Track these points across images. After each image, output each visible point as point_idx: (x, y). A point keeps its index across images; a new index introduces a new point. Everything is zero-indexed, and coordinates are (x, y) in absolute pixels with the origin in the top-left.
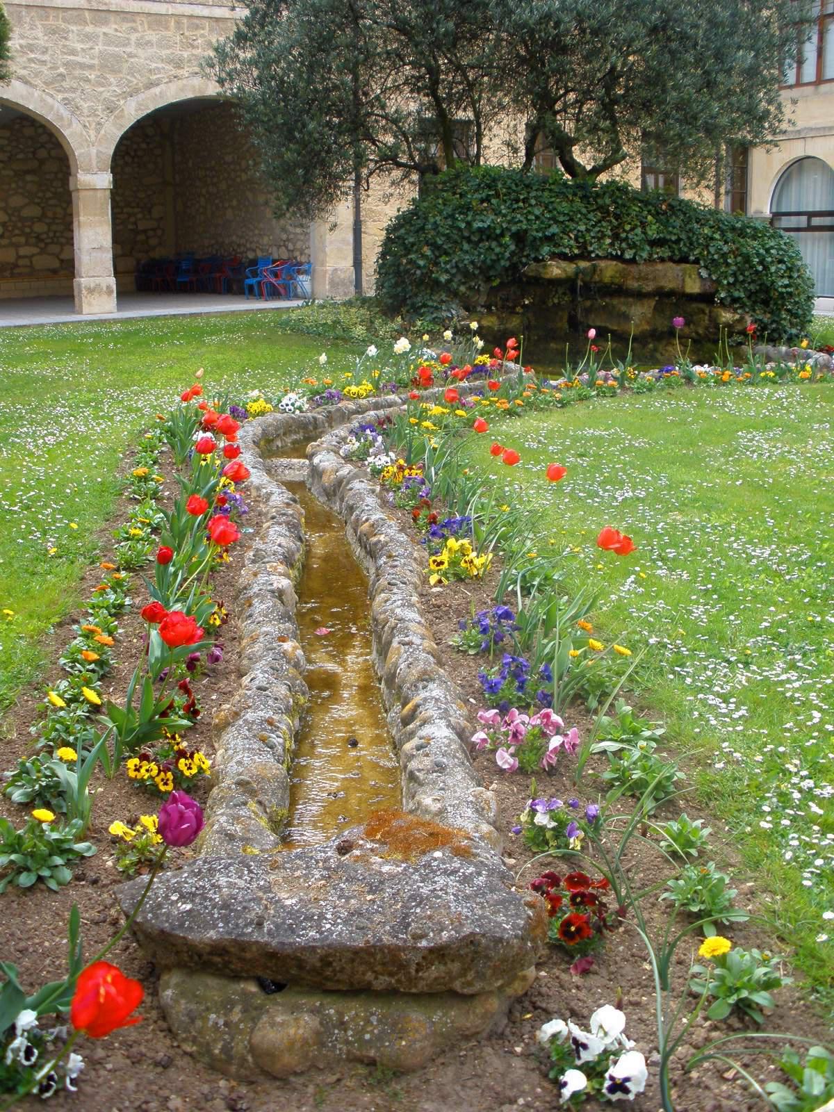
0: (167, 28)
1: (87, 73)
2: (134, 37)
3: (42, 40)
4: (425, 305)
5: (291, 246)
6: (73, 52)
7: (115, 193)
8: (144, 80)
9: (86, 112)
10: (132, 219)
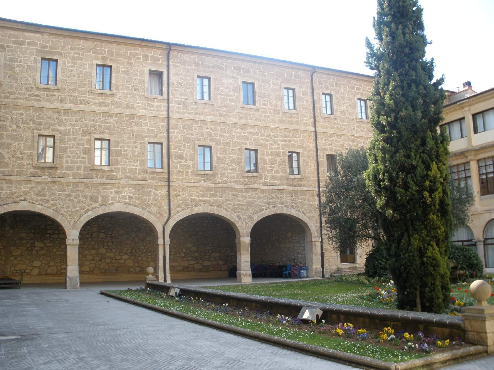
0: (266, 193)
1: (243, 207)
2: (256, 196)
3: (231, 197)
4: (383, 274)
5: (296, 261)
6: (240, 201)
7: (252, 244)
8: (259, 209)
9: (243, 219)
10: (227, 252)
